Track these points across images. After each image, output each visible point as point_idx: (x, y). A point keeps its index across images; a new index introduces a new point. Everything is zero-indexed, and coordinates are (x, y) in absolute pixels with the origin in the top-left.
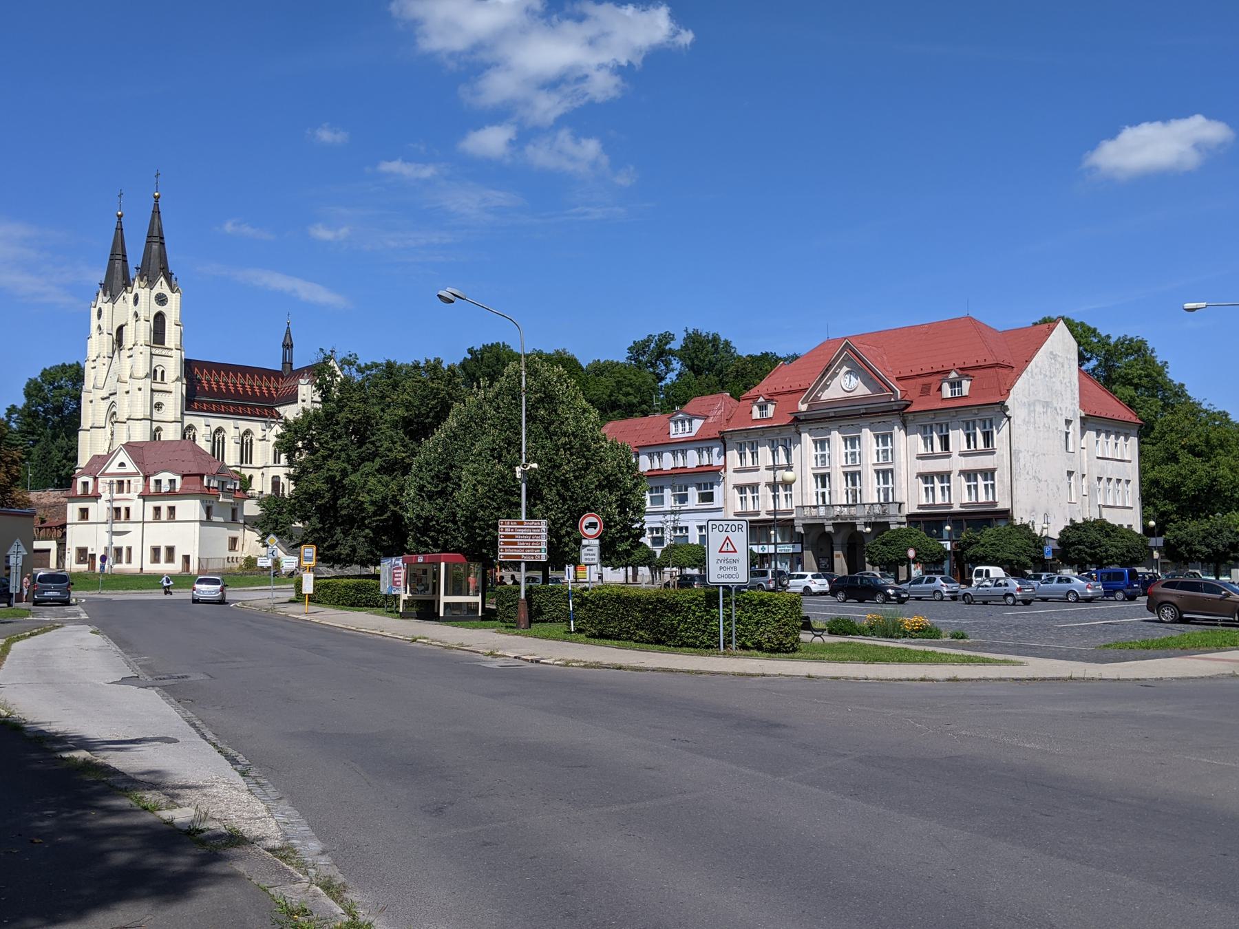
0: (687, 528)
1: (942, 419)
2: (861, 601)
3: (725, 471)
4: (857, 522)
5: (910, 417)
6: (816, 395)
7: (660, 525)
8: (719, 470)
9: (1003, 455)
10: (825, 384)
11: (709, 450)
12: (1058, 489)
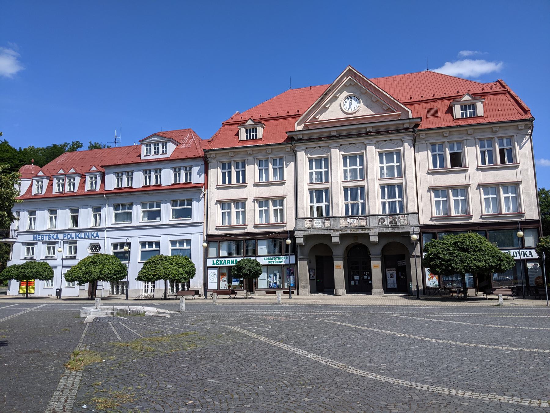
4: (371, 232)
6: (314, 117)
7: (123, 241)
8: (201, 187)
9: (527, 170)
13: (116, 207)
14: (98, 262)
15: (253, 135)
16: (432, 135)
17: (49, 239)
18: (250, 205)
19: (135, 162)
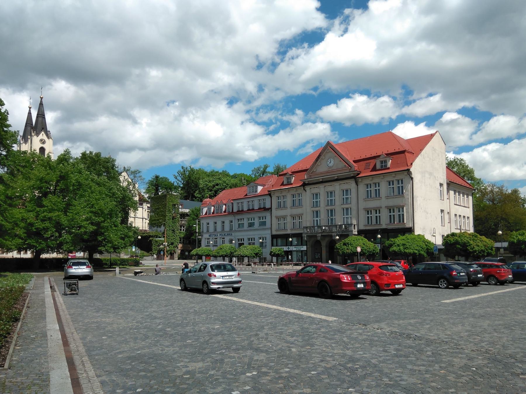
12: (436, 218)
15: (385, 165)
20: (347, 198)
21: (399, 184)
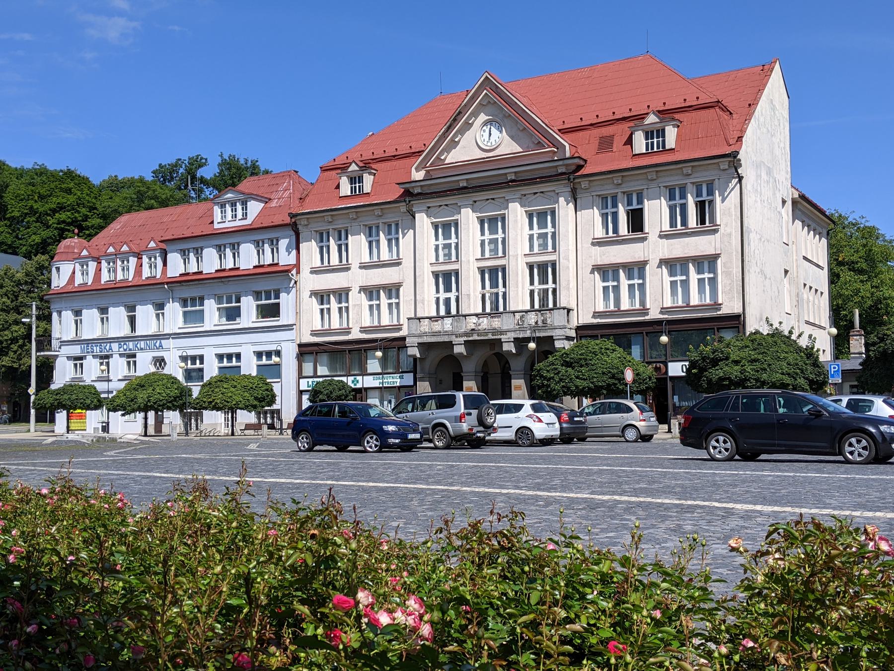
0: (201, 358)
1: (633, 186)
2: (342, 449)
3: (298, 272)
4: (503, 338)
5: (584, 184)
6: (438, 158)
7: (273, 347)
8: (289, 271)
9: (730, 235)
10: (452, 140)
11: (274, 243)
13: (184, 302)
14: (147, 385)
15: (359, 186)
16: (598, 183)
17: (101, 352)
18: (357, 299)
19: (277, 224)
20: (543, 236)
21: (607, 208)
